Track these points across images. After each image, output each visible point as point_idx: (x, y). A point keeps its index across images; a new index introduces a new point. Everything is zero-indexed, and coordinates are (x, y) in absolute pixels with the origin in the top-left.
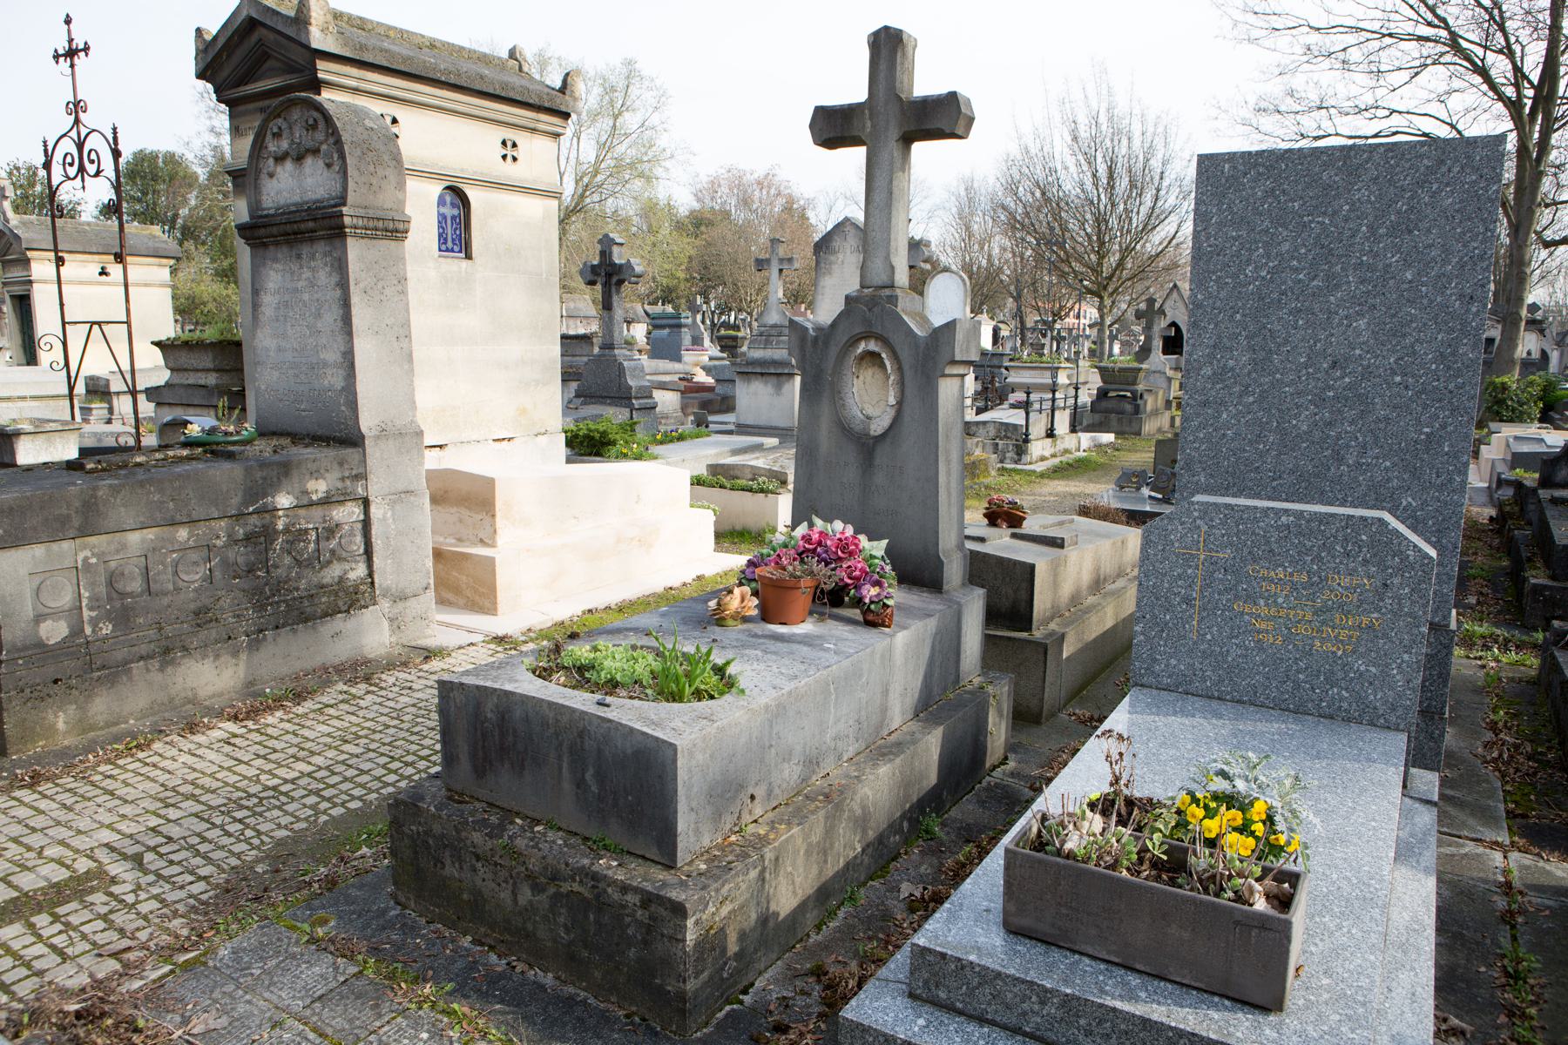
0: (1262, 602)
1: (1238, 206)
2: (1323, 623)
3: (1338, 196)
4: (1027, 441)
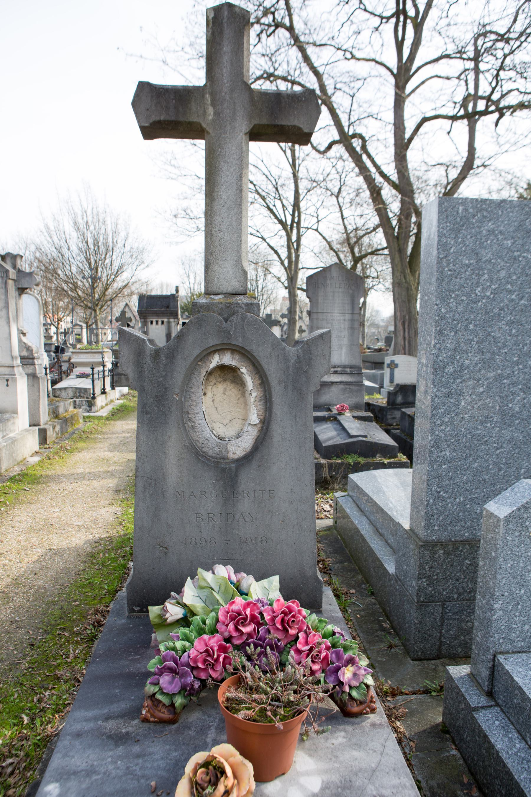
1: (469, 241)
4: (94, 398)
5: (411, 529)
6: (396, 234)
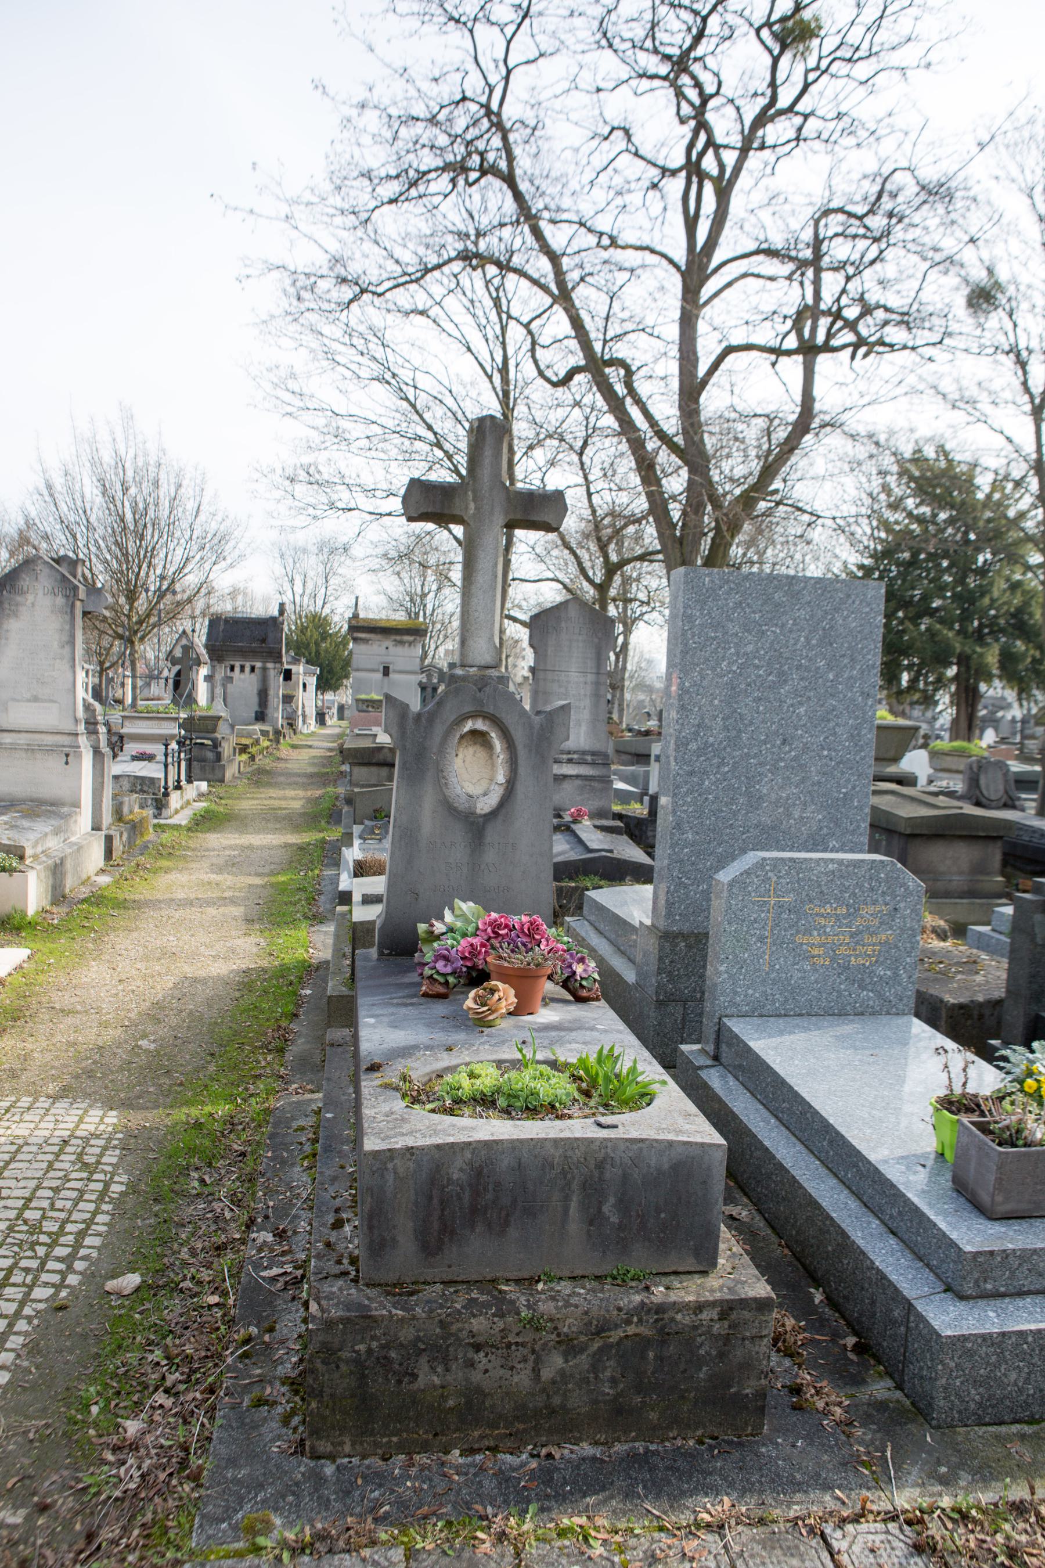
0: (815, 933)
2: (857, 943)
3: (784, 613)
4: (166, 794)
5: (653, 925)
6: (678, 533)
